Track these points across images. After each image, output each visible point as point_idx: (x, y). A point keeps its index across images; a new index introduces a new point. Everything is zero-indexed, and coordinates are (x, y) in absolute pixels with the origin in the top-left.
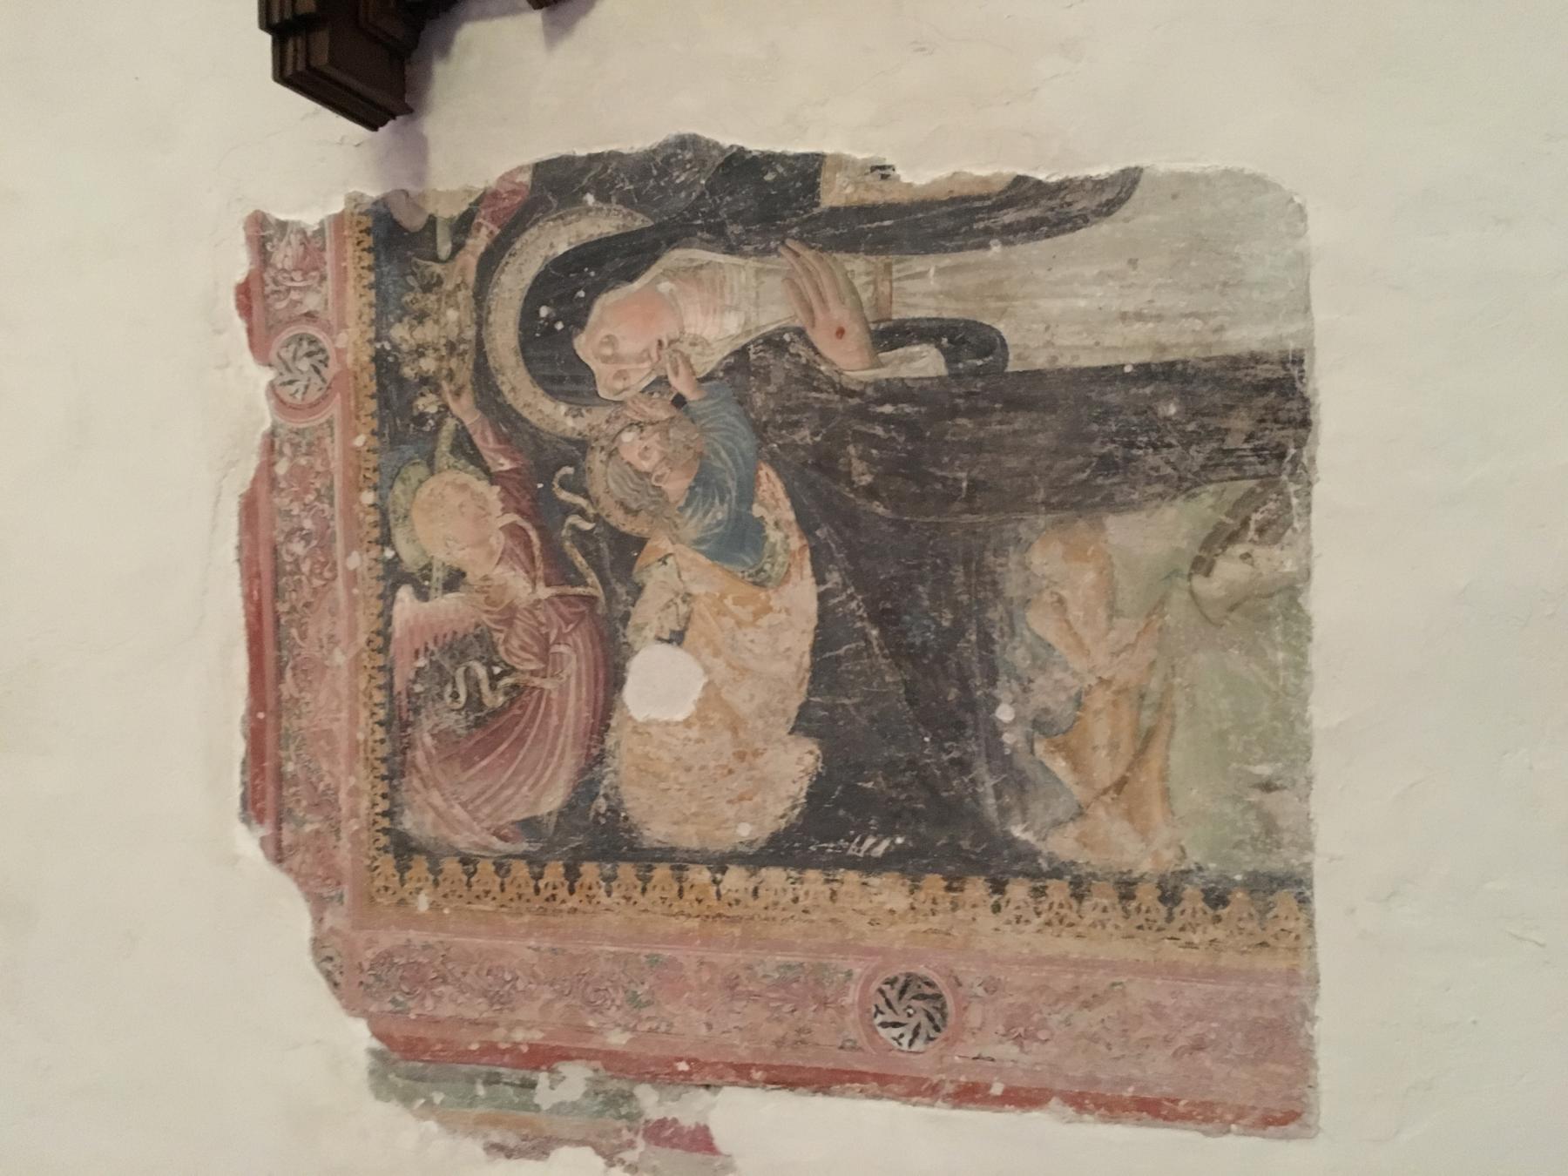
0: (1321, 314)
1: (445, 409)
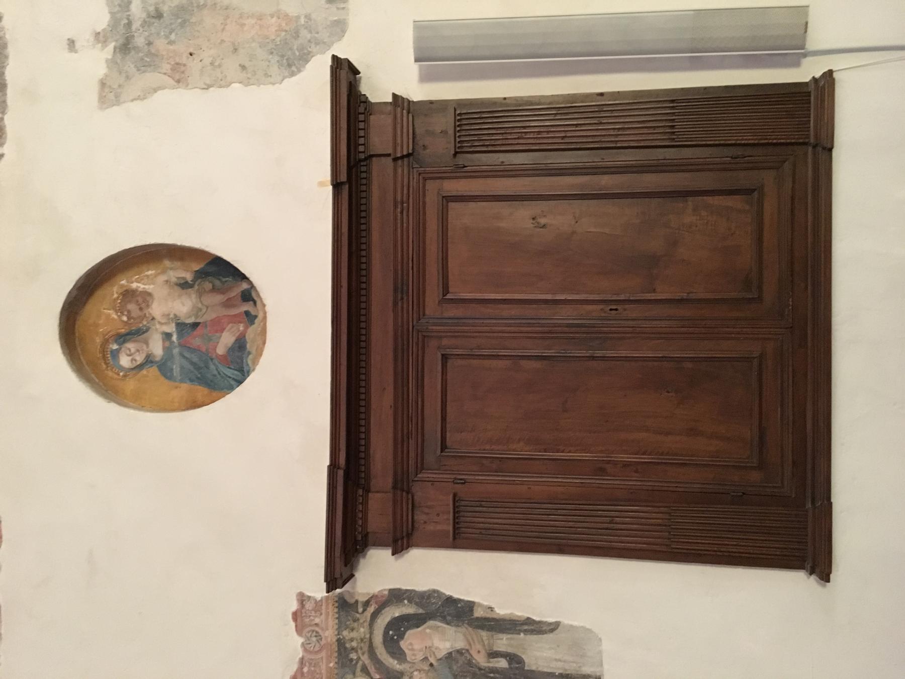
0: (606, 666)
1: (359, 659)
